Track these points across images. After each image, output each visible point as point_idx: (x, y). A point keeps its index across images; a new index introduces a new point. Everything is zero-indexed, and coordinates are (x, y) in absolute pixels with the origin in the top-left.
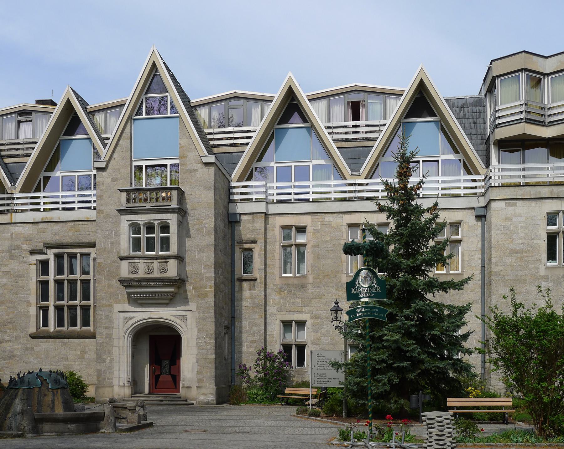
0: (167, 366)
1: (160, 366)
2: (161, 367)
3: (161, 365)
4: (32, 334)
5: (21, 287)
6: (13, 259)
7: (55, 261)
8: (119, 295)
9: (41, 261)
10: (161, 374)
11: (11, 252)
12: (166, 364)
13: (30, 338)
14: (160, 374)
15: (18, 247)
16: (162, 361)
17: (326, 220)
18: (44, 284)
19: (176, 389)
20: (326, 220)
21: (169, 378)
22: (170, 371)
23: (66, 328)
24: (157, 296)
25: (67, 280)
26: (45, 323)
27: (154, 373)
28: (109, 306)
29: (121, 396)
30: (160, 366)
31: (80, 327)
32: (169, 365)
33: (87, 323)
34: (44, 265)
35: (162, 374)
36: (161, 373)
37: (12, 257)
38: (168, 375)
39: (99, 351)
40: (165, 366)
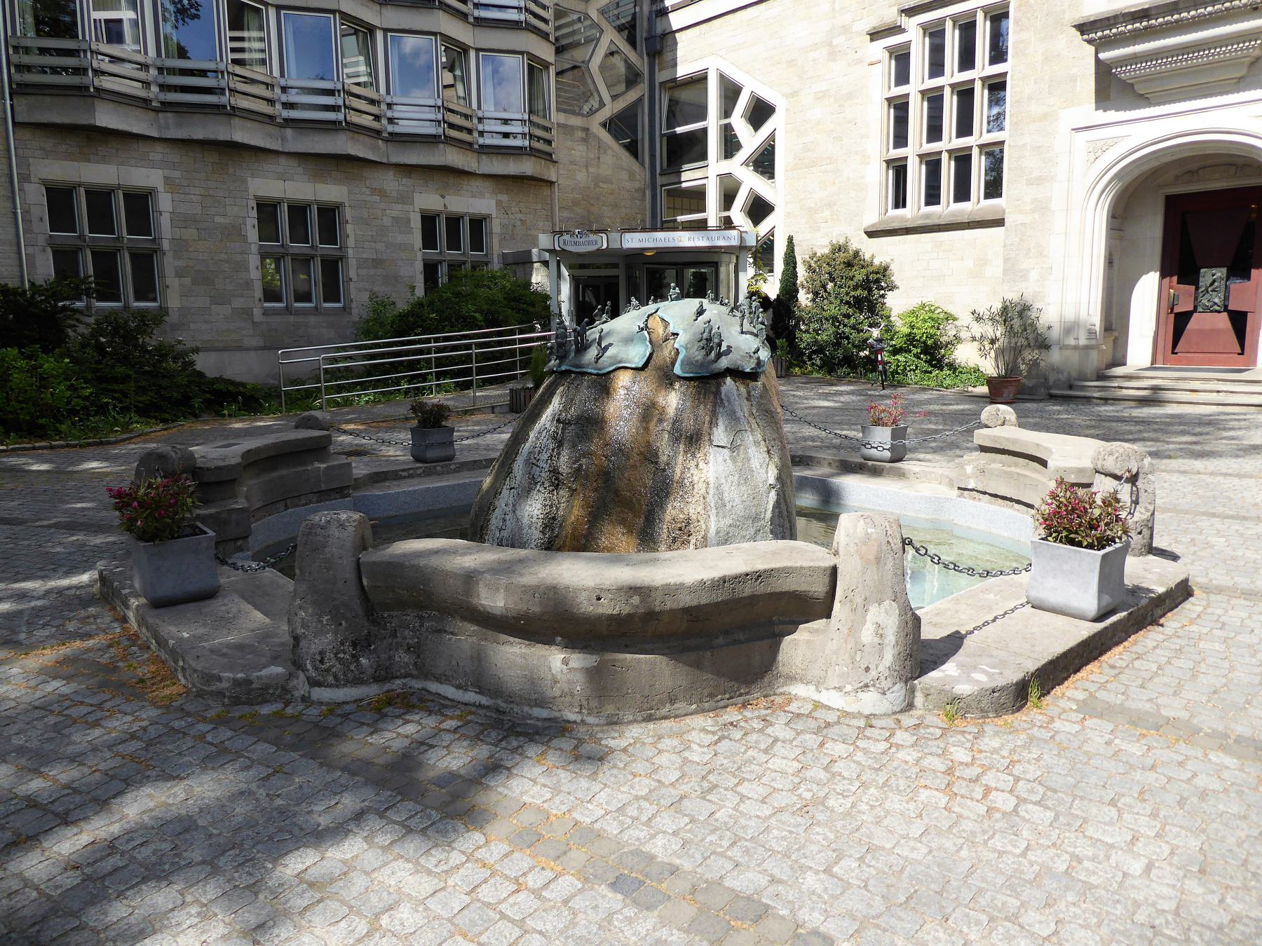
0: (1216, 284)
1: (1194, 287)
2: (1197, 288)
3: (1195, 282)
4: (868, 227)
5: (849, 122)
6: (834, 60)
7: (924, 44)
8: (1075, 81)
9: (891, 51)
10: (1195, 310)
11: (830, 45)
12: (1214, 281)
13: (865, 236)
14: (1192, 308)
15: (846, 29)
16: (1203, 270)
17: (1248, 581)
18: (900, 108)
19: (1242, 354)
20: (1248, 581)
21: (1223, 321)
22: (1226, 298)
23: (948, 207)
24: (1202, 57)
25: (951, 85)
26: (900, 201)
27: (1172, 309)
28: (1045, 116)
29: (1065, 374)
30: (1194, 287)
31: (976, 201)
32: (1223, 282)
33: (994, 188)
34: (901, 58)
35: (1200, 309)
36: (1195, 307)
37: (833, 54)
38: (1219, 312)
39: (1012, 250)
40: (1212, 284)
